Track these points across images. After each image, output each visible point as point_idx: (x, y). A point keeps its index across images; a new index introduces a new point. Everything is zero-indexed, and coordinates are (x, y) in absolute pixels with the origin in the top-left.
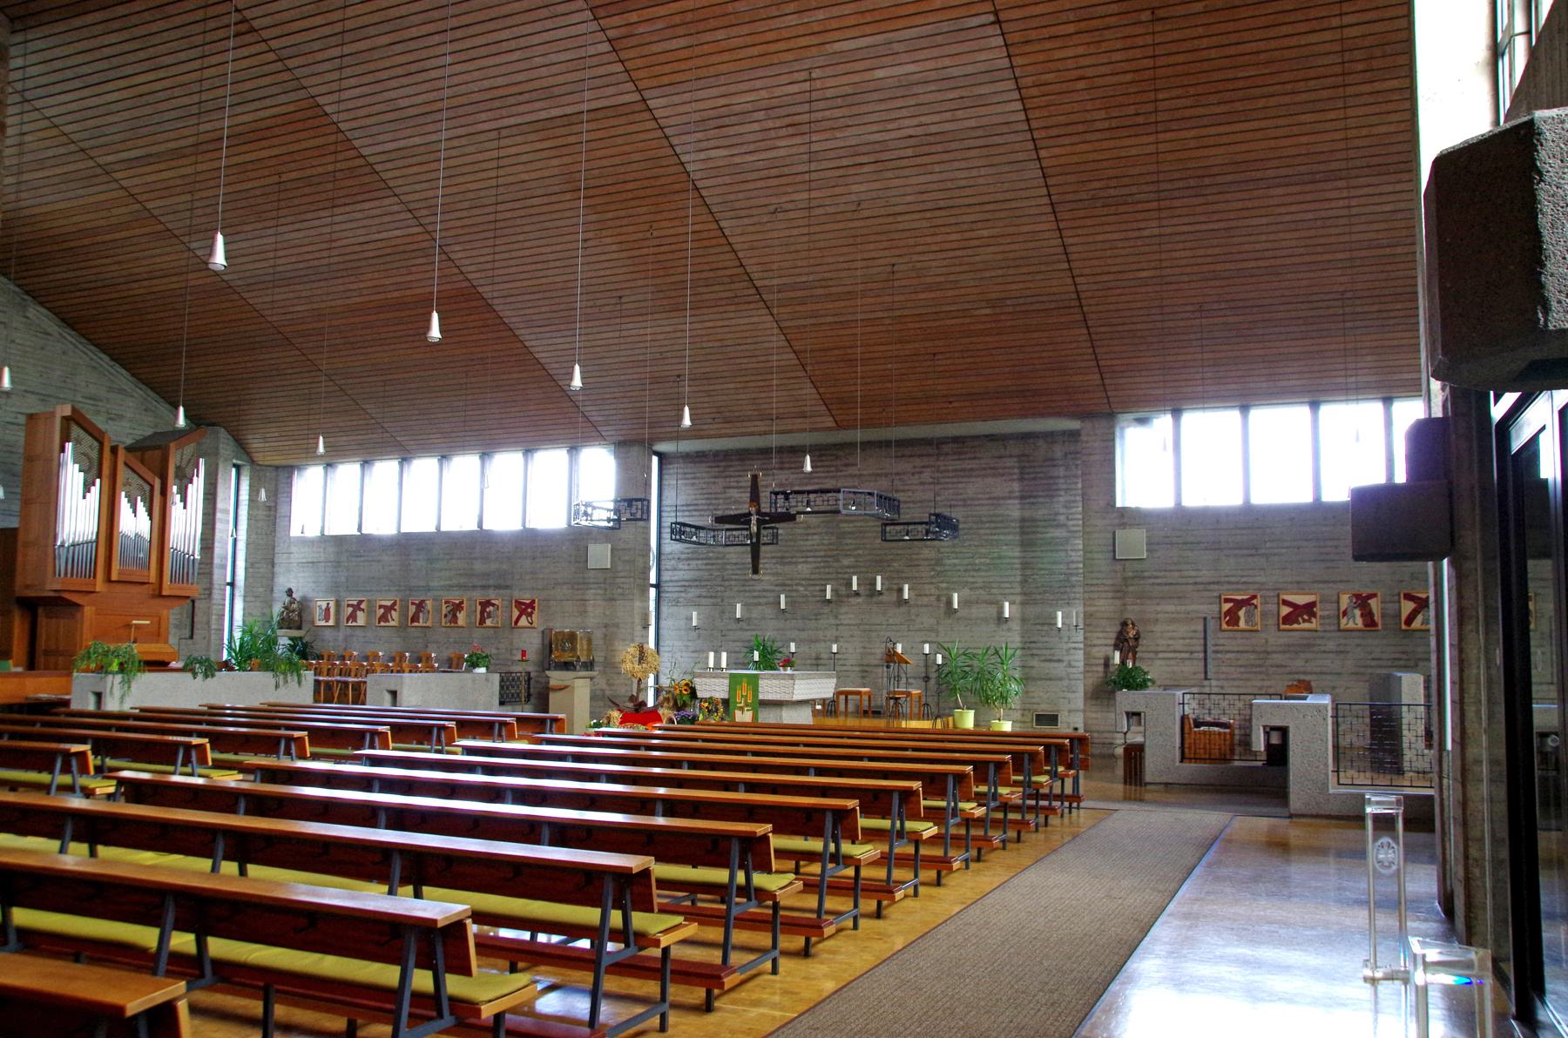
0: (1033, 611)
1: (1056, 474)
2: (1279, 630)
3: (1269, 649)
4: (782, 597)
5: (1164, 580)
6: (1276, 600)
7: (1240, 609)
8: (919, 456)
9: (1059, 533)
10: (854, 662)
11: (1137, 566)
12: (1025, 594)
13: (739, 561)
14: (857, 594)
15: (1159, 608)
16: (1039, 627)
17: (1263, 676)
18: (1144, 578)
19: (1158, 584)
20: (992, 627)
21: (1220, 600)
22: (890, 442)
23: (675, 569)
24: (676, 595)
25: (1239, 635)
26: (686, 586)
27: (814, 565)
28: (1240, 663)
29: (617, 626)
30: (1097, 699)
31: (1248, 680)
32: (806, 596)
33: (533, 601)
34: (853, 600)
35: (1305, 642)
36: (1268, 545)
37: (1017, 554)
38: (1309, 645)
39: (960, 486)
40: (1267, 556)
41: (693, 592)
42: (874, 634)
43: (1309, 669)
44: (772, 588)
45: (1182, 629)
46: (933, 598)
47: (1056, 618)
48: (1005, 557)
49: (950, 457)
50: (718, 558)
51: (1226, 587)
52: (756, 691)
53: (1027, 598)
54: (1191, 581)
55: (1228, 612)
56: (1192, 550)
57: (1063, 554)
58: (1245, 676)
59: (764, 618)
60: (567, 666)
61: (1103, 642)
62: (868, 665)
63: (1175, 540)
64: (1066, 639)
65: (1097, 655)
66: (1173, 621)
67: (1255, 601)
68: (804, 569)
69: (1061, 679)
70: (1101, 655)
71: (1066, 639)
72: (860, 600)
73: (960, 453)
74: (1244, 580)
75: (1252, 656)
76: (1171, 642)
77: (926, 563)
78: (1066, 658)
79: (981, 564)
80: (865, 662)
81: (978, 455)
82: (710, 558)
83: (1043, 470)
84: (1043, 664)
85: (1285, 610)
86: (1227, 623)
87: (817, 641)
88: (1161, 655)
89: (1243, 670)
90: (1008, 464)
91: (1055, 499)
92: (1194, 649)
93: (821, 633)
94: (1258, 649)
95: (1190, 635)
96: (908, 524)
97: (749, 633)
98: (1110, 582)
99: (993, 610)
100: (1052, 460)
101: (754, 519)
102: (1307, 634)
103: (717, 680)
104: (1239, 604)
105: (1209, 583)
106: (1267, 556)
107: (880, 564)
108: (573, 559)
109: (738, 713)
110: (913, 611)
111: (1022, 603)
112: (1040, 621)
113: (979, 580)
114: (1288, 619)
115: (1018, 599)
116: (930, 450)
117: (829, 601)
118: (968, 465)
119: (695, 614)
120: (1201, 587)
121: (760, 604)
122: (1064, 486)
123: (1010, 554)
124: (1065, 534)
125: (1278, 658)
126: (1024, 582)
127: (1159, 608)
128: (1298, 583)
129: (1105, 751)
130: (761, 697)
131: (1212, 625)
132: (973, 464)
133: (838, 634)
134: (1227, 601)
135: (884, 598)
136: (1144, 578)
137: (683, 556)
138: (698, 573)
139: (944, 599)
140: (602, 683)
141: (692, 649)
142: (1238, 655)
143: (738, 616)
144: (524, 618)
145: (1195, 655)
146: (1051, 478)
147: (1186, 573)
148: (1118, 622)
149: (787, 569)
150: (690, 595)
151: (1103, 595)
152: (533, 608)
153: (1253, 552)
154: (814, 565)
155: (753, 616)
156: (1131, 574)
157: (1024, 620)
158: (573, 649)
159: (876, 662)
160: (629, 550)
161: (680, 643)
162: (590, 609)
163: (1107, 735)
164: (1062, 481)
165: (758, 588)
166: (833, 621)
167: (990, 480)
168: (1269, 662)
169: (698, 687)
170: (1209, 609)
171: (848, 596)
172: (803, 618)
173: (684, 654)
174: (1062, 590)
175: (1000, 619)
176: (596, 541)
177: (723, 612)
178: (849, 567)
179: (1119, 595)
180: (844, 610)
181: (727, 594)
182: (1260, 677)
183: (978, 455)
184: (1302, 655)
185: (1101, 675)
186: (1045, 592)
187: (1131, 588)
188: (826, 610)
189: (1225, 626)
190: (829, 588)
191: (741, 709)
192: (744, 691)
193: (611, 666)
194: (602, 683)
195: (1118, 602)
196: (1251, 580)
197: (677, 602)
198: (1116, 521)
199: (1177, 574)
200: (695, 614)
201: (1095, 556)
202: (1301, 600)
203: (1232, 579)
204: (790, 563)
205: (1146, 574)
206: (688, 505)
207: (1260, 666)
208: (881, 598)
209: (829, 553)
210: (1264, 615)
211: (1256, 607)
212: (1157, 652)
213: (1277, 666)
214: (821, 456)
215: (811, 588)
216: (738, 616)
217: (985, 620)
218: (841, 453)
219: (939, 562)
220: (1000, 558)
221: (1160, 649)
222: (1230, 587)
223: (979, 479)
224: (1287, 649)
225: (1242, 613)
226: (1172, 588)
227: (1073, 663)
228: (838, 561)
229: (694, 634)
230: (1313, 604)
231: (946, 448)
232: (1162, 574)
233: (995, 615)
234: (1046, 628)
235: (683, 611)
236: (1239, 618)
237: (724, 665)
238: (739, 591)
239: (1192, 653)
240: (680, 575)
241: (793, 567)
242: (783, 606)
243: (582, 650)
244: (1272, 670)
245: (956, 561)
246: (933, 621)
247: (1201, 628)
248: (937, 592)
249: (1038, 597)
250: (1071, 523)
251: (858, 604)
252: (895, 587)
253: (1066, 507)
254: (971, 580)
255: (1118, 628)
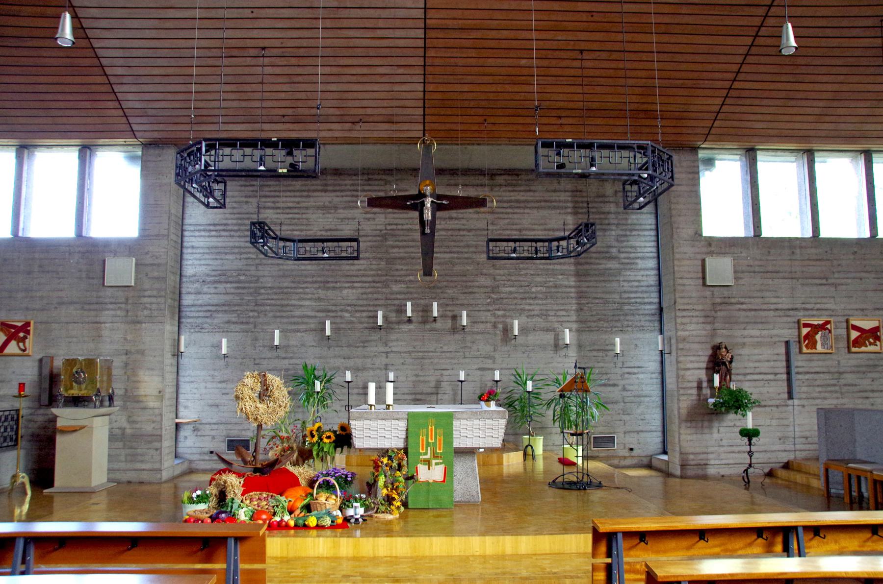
0: (587, 337)
1: (607, 210)
2: (849, 352)
3: (841, 370)
4: (328, 323)
5: (750, 307)
6: (844, 325)
7: (817, 333)
8: (473, 185)
9: (612, 265)
10: (406, 391)
11: (726, 292)
12: (581, 322)
13: (277, 285)
14: (409, 320)
15: (746, 333)
16: (595, 353)
17: (838, 395)
18: (731, 304)
19: (744, 310)
20: (550, 354)
21: (799, 325)
22: (457, 170)
23: (200, 293)
24: (199, 321)
25: (815, 357)
26: (211, 311)
27: (360, 291)
28: (818, 383)
29: (142, 352)
30: (691, 421)
31: (825, 398)
32: (352, 322)
33: (28, 324)
34: (406, 327)
35: (871, 363)
36: (836, 275)
37: (573, 283)
38: (875, 366)
39: (515, 216)
40: (836, 285)
41: (220, 318)
42: (427, 361)
43: (875, 388)
44: (313, 314)
45: (767, 352)
46: (489, 325)
47: (614, 345)
48: (561, 286)
49: (504, 188)
50: (251, 282)
51: (801, 313)
52: (448, 436)
53: (583, 327)
54: (772, 307)
55: (807, 336)
56: (773, 279)
57: (615, 284)
58: (823, 395)
59: (303, 345)
60: (76, 401)
61: (696, 365)
62: (421, 394)
63: (757, 269)
64: (620, 365)
65: (690, 378)
66: (759, 344)
67: (828, 326)
68: (349, 294)
69: (616, 402)
70: (695, 378)
71: (620, 365)
72: (411, 327)
73: (515, 185)
74: (818, 306)
75: (827, 376)
76: (757, 365)
77: (482, 290)
78: (622, 383)
79: (537, 292)
80: (418, 390)
81: (533, 188)
82: (239, 282)
83: (596, 205)
84: (600, 389)
85: (854, 334)
86: (807, 346)
87: (364, 369)
88: (749, 377)
89: (820, 389)
90: (562, 198)
91: (608, 233)
92: (777, 371)
93: (369, 360)
94: (832, 370)
95: (775, 358)
96: (536, 241)
97: (286, 362)
98: (700, 307)
99: (549, 337)
100: (604, 196)
101: (428, 202)
102: (872, 356)
103: (387, 423)
104: (816, 329)
105: (789, 310)
106: (836, 285)
107: (434, 292)
108: (84, 275)
109: (422, 469)
110: (469, 338)
111: (578, 331)
112: (596, 347)
113: (538, 308)
114: (857, 343)
115: (575, 326)
116: (485, 180)
117: (380, 327)
118: (521, 196)
119: (224, 341)
120: (781, 313)
121: (298, 331)
122: (615, 222)
123: (566, 283)
124: (617, 266)
125: (849, 378)
126: (580, 310)
127: (746, 333)
128: (863, 310)
129: (700, 472)
130: (456, 444)
131: (794, 349)
132: (528, 196)
133: (387, 361)
134: (806, 325)
135: (438, 325)
136: (731, 304)
137: (209, 279)
138: (228, 298)
139: (500, 326)
140: (123, 422)
141: (218, 379)
142: (816, 376)
143: (276, 342)
144: (13, 343)
145: (779, 376)
146: (604, 213)
147: (767, 300)
148: (709, 346)
149: (330, 293)
150: (216, 321)
151: (695, 320)
152: (28, 332)
153: (824, 281)
154: (360, 291)
155: (292, 343)
156: (719, 300)
157: (580, 346)
158: (93, 381)
159: (429, 390)
160: (159, 265)
161: (204, 373)
162: (105, 333)
163: (702, 456)
164: (613, 216)
165: (297, 313)
166: (382, 349)
167: (545, 213)
168: (842, 382)
169: (355, 433)
170: (790, 334)
171: (399, 323)
172: (349, 346)
173: (209, 385)
174: (617, 318)
175: (558, 346)
176: (115, 254)
177: (256, 339)
178: (400, 293)
179: (709, 320)
180: (393, 337)
181: (261, 320)
182: (835, 395)
183: (533, 188)
184: (870, 375)
185: (694, 398)
186: (600, 320)
187: (719, 314)
188: (375, 336)
189: (805, 350)
190: (380, 314)
191: (428, 462)
192: (430, 436)
193: (132, 399)
194: (123, 422)
195: (709, 327)
196: (823, 306)
197: (200, 328)
198: (704, 250)
199: (760, 300)
200: (224, 341)
201: (685, 281)
202: (867, 325)
203: (808, 306)
204: (334, 288)
205: (733, 300)
206: (214, 225)
207: (834, 385)
208: (434, 325)
209: (377, 279)
210: (837, 338)
211: (830, 331)
212: (745, 374)
213: (849, 385)
214: (369, 179)
215: (358, 315)
216: (276, 342)
217: (543, 347)
218: (389, 178)
219: (494, 289)
220: (556, 287)
221: (748, 371)
222: (807, 313)
223: (535, 211)
224: (858, 370)
225: (818, 337)
226: (757, 313)
227: (628, 387)
228: (387, 286)
229: (222, 362)
230: (877, 329)
231: (500, 180)
232: (747, 300)
233: (552, 342)
234: (601, 354)
235: (209, 338)
236: (816, 342)
237: (390, 400)
238: (275, 317)
239: (776, 374)
240: (204, 299)
241: (337, 292)
242: (328, 333)
243: (102, 381)
244: (845, 389)
245: (512, 289)
246: (489, 348)
247: (782, 350)
248: (493, 320)
249: (593, 324)
250: (622, 255)
251: (410, 331)
252: (450, 314)
253: (618, 241)
254: (527, 307)
255: (710, 352)
